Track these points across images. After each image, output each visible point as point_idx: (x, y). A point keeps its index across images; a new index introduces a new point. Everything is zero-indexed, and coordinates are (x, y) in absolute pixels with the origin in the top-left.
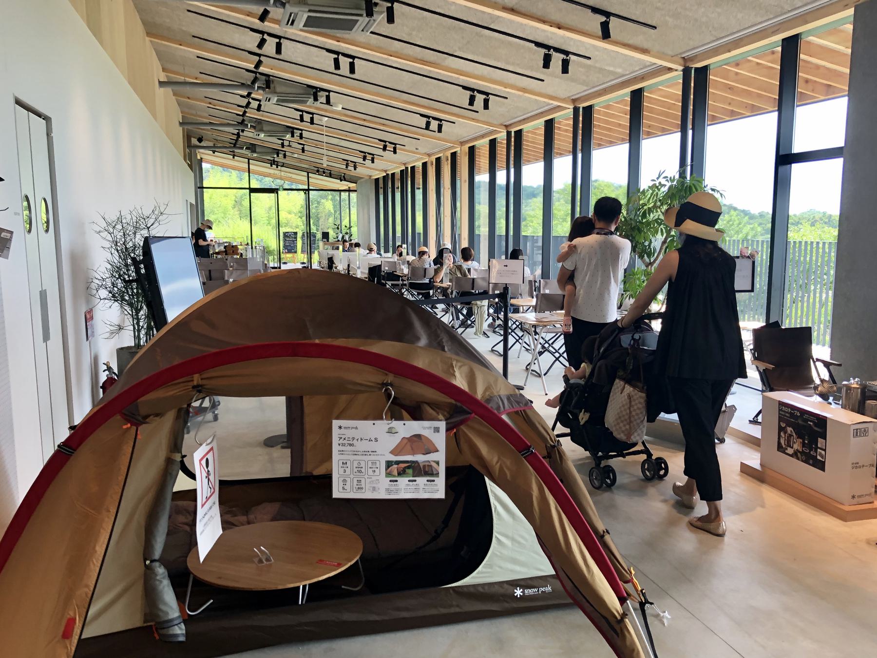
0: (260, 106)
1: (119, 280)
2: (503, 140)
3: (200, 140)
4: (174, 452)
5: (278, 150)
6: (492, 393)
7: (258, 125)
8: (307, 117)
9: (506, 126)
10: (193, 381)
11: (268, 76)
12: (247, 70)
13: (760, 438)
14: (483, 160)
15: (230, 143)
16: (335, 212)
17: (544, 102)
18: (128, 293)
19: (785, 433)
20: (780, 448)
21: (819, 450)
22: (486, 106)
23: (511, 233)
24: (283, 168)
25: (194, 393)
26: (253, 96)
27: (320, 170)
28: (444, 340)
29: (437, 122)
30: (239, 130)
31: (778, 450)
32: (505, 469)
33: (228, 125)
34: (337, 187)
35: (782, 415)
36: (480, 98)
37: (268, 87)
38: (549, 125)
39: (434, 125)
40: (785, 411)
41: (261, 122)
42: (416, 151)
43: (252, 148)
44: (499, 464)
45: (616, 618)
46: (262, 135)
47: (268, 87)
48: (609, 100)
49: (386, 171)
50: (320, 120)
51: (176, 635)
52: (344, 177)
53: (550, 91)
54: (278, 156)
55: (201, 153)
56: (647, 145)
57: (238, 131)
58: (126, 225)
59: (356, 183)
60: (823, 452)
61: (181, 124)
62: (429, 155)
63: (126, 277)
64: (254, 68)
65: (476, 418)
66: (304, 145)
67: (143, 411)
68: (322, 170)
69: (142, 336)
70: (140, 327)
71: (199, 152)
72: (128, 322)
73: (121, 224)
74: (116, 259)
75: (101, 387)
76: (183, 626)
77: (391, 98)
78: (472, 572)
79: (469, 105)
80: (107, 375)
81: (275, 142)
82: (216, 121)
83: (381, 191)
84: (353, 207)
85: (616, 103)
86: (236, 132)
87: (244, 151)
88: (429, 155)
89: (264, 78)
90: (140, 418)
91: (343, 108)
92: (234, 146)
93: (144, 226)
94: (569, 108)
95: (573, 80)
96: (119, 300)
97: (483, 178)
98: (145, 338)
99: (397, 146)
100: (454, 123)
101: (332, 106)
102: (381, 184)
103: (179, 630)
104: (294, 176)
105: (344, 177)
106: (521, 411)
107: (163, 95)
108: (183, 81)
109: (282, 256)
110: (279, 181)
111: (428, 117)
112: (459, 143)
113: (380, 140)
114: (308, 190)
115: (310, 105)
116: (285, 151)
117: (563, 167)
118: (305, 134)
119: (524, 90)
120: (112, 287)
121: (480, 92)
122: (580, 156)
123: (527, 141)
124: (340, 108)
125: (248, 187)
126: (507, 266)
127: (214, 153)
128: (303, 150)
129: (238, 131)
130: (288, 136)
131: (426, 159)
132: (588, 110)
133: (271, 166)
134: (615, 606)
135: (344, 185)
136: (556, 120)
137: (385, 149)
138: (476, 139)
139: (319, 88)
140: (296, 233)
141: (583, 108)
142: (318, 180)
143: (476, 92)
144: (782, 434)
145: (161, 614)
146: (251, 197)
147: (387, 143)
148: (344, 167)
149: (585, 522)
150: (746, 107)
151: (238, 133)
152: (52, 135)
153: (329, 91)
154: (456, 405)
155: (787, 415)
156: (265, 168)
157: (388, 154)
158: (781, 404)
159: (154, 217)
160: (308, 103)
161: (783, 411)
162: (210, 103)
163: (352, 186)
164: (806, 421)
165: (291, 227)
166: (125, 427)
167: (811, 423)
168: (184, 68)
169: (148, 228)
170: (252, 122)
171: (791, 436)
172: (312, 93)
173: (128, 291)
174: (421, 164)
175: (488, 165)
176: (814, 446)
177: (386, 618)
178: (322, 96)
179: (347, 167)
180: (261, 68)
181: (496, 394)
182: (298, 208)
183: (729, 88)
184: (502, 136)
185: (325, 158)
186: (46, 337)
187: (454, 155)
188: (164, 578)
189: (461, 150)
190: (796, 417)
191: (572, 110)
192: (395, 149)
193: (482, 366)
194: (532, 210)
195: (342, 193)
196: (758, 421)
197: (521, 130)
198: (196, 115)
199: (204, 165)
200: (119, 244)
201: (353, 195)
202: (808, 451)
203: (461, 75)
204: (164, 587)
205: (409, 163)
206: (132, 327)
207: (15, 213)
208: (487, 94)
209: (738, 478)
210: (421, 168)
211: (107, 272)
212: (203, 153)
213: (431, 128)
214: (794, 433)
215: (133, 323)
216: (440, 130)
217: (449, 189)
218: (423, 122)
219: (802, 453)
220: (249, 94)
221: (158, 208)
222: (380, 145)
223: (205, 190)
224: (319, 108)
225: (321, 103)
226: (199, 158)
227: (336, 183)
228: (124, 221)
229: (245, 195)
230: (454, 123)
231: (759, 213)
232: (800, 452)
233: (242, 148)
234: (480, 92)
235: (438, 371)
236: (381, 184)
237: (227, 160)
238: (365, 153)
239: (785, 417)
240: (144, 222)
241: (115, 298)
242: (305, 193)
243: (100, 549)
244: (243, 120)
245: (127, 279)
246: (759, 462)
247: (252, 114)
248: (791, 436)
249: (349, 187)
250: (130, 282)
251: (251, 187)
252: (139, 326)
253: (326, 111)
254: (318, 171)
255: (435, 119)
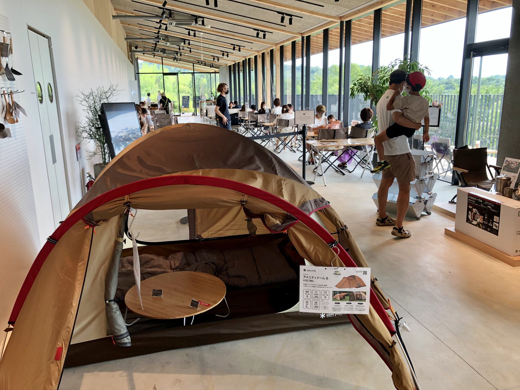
0: (166, 27)
1: (93, 127)
2: (300, 41)
3: (136, 48)
4: (119, 237)
5: (177, 52)
6: (306, 199)
7: (167, 38)
8: (192, 33)
9: (301, 34)
10: (124, 200)
11: (170, 10)
12: (159, 8)
13: (455, 213)
14: (288, 53)
15: (152, 49)
16: (208, 84)
17: (324, 19)
18: (98, 134)
19: (472, 212)
20: (468, 220)
21: (494, 223)
22: (291, 23)
23: (304, 93)
24: (180, 62)
25: (125, 208)
26: (162, 22)
27: (200, 62)
28: (276, 166)
29: (263, 33)
30: (156, 41)
31: (466, 222)
32: (318, 253)
33: (151, 39)
34: (209, 71)
35: (470, 201)
36: (287, 18)
37: (170, 16)
38: (326, 32)
39: (261, 34)
40: (472, 199)
41: (167, 37)
42: (251, 49)
43: (164, 51)
44: (314, 251)
45: (388, 344)
46: (168, 44)
47: (170, 16)
48: (360, 17)
49: (235, 61)
50: (199, 34)
51: (126, 343)
52: (212, 65)
53: (327, 13)
54: (177, 55)
55: (137, 55)
56: (384, 42)
57: (156, 42)
58: (95, 96)
59: (219, 68)
60: (497, 224)
61: (126, 39)
62: (258, 52)
63: (97, 125)
64: (163, 6)
65: (300, 222)
66: (191, 48)
67: (96, 218)
68: (201, 62)
69: (106, 158)
70: (106, 153)
71: (136, 54)
72: (99, 150)
73: (92, 96)
74: (91, 115)
75: (86, 186)
76: (129, 337)
77: (237, 20)
78: (295, 305)
79: (281, 22)
80: (89, 179)
81: (175, 47)
82: (144, 37)
83: (232, 72)
84: (217, 81)
85: (364, 18)
86: (154, 42)
87: (160, 53)
88: (258, 52)
89: (168, 12)
90: (94, 222)
91: (211, 27)
92: (154, 50)
93: (105, 97)
94: (338, 22)
95: (340, 5)
96: (94, 138)
97: (288, 63)
98: (108, 159)
99: (241, 47)
100: (272, 33)
101: (205, 26)
102: (232, 69)
103: (127, 340)
104: (186, 66)
105: (212, 65)
106: (323, 209)
107: (115, 23)
108: (125, 15)
109: (181, 109)
110: (178, 68)
111: (258, 30)
112: (275, 45)
113: (232, 44)
114: (194, 73)
115: (193, 26)
116: (181, 52)
117: (334, 56)
118: (191, 42)
119: (312, 12)
120: (90, 131)
121: (287, 15)
122: (344, 49)
123: (313, 42)
124: (209, 27)
125: (162, 72)
126: (305, 114)
127: (144, 54)
128: (190, 51)
129: (156, 42)
130: (182, 44)
131: (256, 54)
132: (349, 23)
133: (174, 60)
134: (389, 338)
135: (213, 70)
136: (330, 29)
137: (234, 49)
138: (284, 42)
139: (198, 16)
140: (189, 97)
141: (346, 22)
142: (199, 68)
143: (285, 14)
144: (470, 212)
145: (116, 331)
146: (164, 77)
147: (235, 46)
148: (212, 60)
149: (374, 292)
150: (442, 17)
151: (156, 43)
152: (52, 47)
153: (203, 18)
154: (287, 215)
155: (473, 201)
156: (170, 62)
157: (236, 52)
158: (470, 195)
159: (110, 92)
160: (192, 25)
161: (471, 199)
162: (140, 27)
163: (217, 70)
164: (487, 205)
165: (185, 93)
166: (86, 228)
167: (490, 207)
168: (125, 8)
169: (107, 98)
170: (162, 37)
171: (475, 214)
172: (194, 19)
173: (98, 133)
174: (253, 57)
175: (291, 56)
176: (491, 220)
177: (245, 332)
178: (200, 21)
179: (214, 60)
180: (166, 6)
181: (307, 200)
182: (189, 83)
183: (433, 6)
184: (299, 39)
185: (202, 55)
186: (54, 161)
187: (272, 51)
188: (117, 310)
189: (276, 48)
190: (480, 203)
191: (340, 23)
192: (239, 49)
193: (299, 182)
194: (316, 80)
195: (212, 74)
196: (455, 202)
197: (310, 35)
198: (133, 34)
199: (139, 61)
200: (92, 107)
201: (217, 75)
202: (487, 223)
203: (276, 5)
204: (117, 316)
205: (247, 56)
206: (101, 153)
207: (31, 92)
208: (291, 16)
209: (444, 238)
210: (254, 58)
211: (86, 123)
212: (138, 55)
213: (259, 36)
214: (478, 212)
215: (102, 150)
216: (264, 37)
217: (269, 70)
218: (255, 33)
219: (483, 224)
220: (161, 21)
221: (112, 87)
222: (231, 47)
223: (140, 74)
224: (198, 28)
225: (199, 24)
226: (136, 57)
227: (208, 69)
228: (94, 95)
229: (161, 76)
230: (272, 33)
231: (438, 79)
232: (481, 223)
233: (158, 51)
234: (287, 15)
235: (272, 190)
236: (232, 69)
237: (150, 57)
238: (223, 52)
239: (472, 203)
240: (105, 95)
241: (91, 137)
242: (192, 75)
243: (75, 304)
244: (158, 36)
245: (97, 127)
246: (454, 228)
247: (162, 32)
248: (475, 214)
249: (215, 71)
250: (99, 128)
251: (164, 72)
252: (104, 152)
253: (202, 29)
254: (199, 62)
255: (261, 31)
